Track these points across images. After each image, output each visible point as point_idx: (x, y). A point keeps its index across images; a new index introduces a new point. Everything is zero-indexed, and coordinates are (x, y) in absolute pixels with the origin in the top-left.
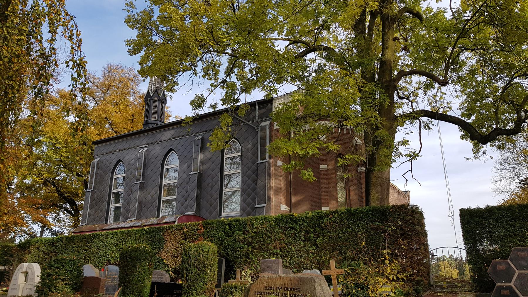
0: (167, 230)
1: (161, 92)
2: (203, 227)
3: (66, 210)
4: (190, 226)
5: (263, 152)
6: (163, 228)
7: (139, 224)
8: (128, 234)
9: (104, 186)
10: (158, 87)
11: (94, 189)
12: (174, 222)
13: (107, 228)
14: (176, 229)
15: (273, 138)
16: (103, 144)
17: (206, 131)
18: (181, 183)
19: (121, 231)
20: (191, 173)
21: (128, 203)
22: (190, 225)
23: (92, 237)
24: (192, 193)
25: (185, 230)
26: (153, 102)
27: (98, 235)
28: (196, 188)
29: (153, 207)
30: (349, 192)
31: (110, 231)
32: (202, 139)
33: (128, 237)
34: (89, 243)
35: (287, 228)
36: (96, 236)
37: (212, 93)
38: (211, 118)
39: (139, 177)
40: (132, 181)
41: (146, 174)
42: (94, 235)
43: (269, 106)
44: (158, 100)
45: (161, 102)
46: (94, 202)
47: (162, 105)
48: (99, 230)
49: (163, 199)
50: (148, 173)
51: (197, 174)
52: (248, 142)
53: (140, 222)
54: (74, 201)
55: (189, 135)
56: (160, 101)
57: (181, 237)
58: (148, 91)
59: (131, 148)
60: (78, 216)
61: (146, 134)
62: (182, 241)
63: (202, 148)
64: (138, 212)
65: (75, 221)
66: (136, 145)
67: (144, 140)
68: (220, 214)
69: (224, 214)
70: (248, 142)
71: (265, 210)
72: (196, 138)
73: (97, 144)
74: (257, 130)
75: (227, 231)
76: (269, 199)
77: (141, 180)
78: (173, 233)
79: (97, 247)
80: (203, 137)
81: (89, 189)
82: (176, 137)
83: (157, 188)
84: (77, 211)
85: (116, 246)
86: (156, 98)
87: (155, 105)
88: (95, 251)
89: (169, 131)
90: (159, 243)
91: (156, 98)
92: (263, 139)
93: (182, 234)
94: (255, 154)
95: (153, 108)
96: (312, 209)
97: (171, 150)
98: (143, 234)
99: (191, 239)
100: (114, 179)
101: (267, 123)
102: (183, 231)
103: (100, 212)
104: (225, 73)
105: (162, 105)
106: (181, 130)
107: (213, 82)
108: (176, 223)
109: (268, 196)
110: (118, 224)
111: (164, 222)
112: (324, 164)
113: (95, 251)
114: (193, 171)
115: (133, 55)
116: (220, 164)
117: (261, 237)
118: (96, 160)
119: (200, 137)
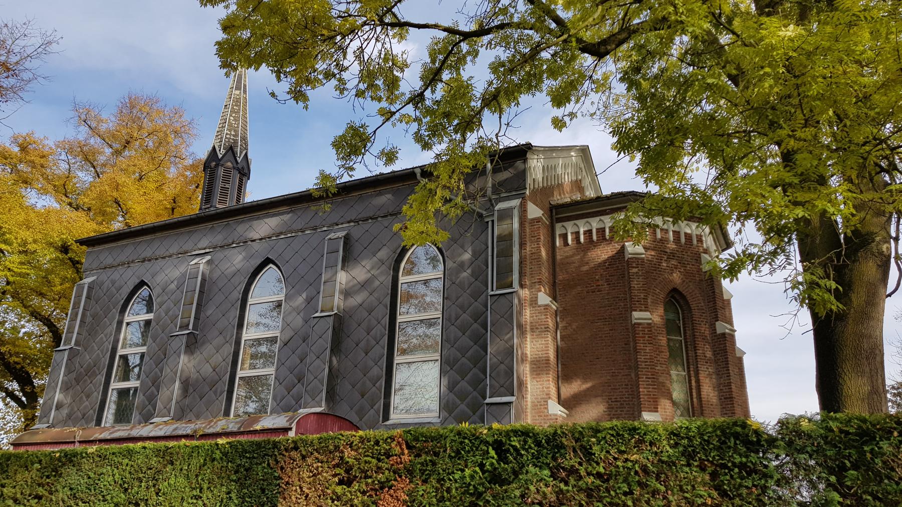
0: (286, 450)
1: (241, 153)
2: (409, 447)
3: (11, 394)
4: (362, 442)
5: (504, 272)
6: (275, 445)
7: (189, 432)
8: (168, 457)
9: (102, 338)
10: (236, 142)
11: (75, 344)
12: (286, 430)
13: (102, 436)
14: (316, 450)
15: (527, 239)
16: (107, 246)
17: (356, 221)
18: (287, 339)
19: (144, 448)
20: (316, 315)
21: (155, 383)
22: (362, 440)
23: (59, 459)
24: (318, 362)
25: (349, 455)
26: (221, 171)
27: (75, 455)
28: (328, 351)
29: (215, 393)
30: (698, 381)
31: (113, 445)
32: (347, 239)
33: (165, 466)
34: (48, 477)
35: (724, 466)
36: (70, 459)
37: (388, 124)
38: (370, 191)
39: (186, 320)
40: (167, 331)
41: (202, 315)
42: (66, 455)
43: (519, 164)
44: (234, 168)
45: (240, 173)
46: (74, 375)
47: (241, 180)
48: (80, 442)
49: (240, 374)
50: (209, 312)
51: (332, 318)
52: (462, 247)
53: (192, 426)
54: (27, 373)
55: (315, 229)
56: (238, 169)
57: (335, 475)
58: (214, 148)
59: (170, 256)
60: (34, 408)
61: (209, 225)
62: (339, 489)
63: (344, 260)
64: (177, 402)
65: (26, 419)
66: (185, 248)
67: (205, 239)
68: (386, 417)
69: (395, 417)
70: (462, 247)
71: (513, 412)
72: (332, 236)
73: (93, 245)
74: (486, 220)
75: (492, 464)
76: (521, 384)
77: (191, 327)
78: (309, 461)
79: (71, 489)
80: (347, 234)
81: (65, 345)
82: (281, 233)
83: (229, 349)
84: (33, 397)
85: (126, 490)
86: (229, 164)
87: (226, 180)
88: (63, 501)
89: (267, 220)
90: (263, 490)
91: (229, 164)
92: (506, 239)
93: (337, 466)
94: (479, 275)
95: (219, 184)
96: (612, 414)
97: (267, 261)
98: (213, 460)
99: (367, 484)
100: (124, 325)
101: (516, 203)
102: (342, 458)
103: (84, 398)
104: (422, 78)
105: (241, 180)
106: (296, 217)
107: (384, 104)
108: (292, 434)
109: (518, 377)
110: (131, 429)
111: (258, 427)
112: (641, 311)
113: (63, 501)
114: (322, 311)
115: (209, 7)
116: (389, 297)
117: (625, 494)
118: (87, 281)
119: (341, 234)
